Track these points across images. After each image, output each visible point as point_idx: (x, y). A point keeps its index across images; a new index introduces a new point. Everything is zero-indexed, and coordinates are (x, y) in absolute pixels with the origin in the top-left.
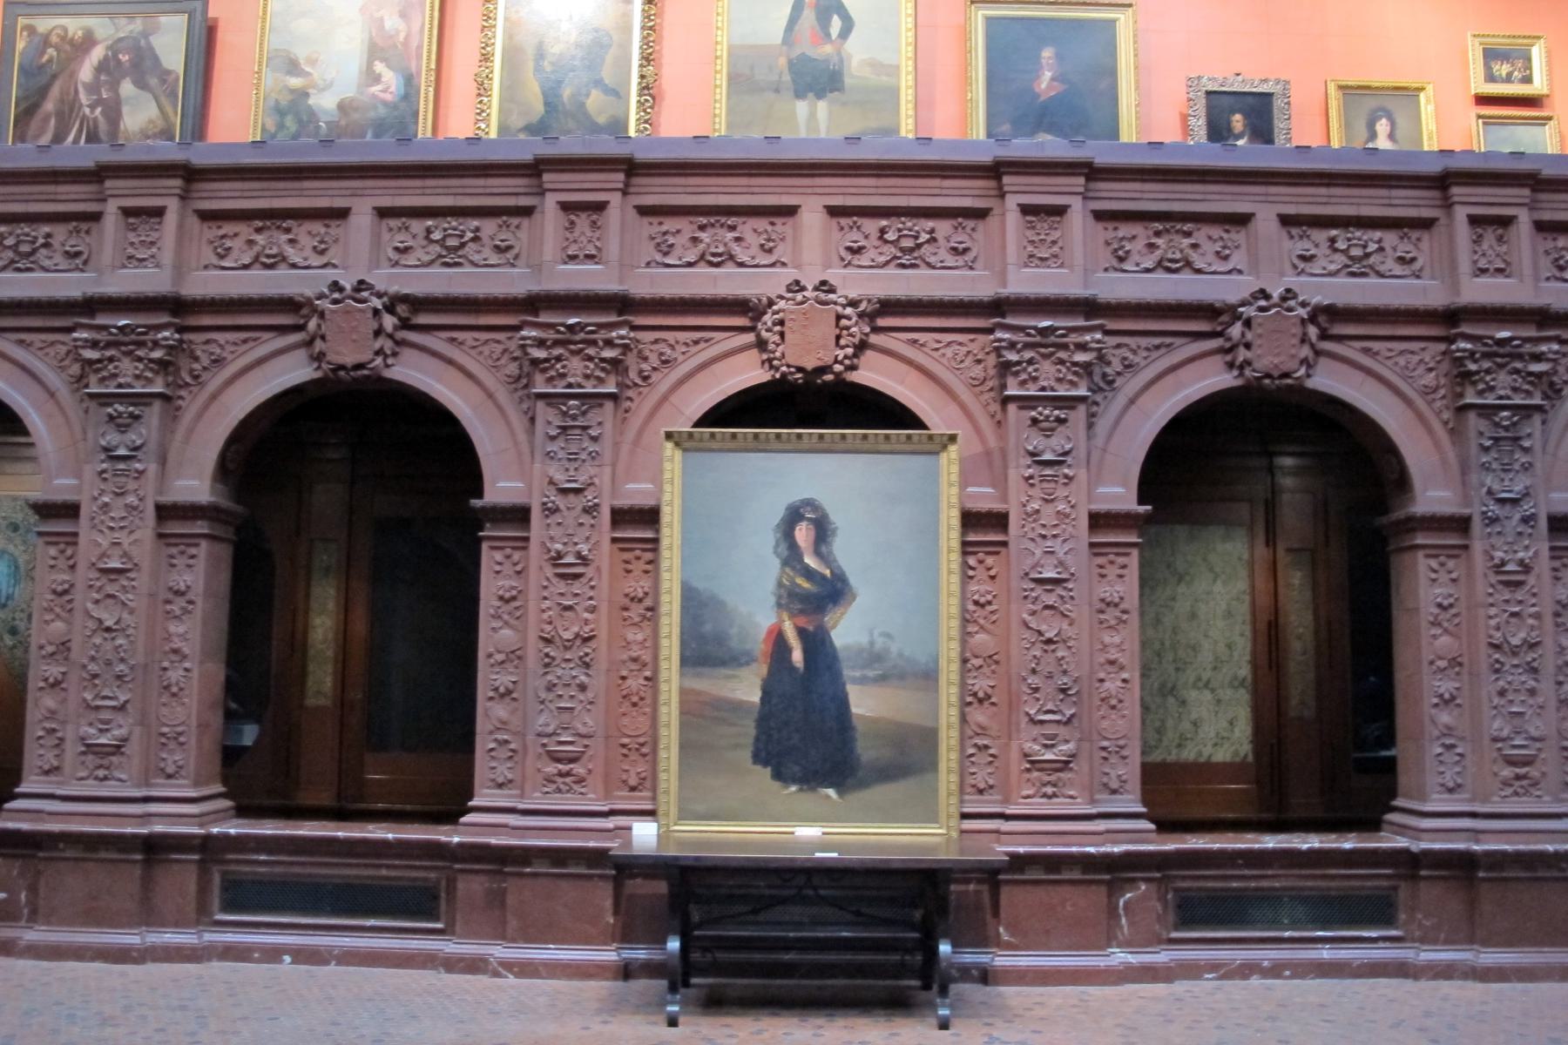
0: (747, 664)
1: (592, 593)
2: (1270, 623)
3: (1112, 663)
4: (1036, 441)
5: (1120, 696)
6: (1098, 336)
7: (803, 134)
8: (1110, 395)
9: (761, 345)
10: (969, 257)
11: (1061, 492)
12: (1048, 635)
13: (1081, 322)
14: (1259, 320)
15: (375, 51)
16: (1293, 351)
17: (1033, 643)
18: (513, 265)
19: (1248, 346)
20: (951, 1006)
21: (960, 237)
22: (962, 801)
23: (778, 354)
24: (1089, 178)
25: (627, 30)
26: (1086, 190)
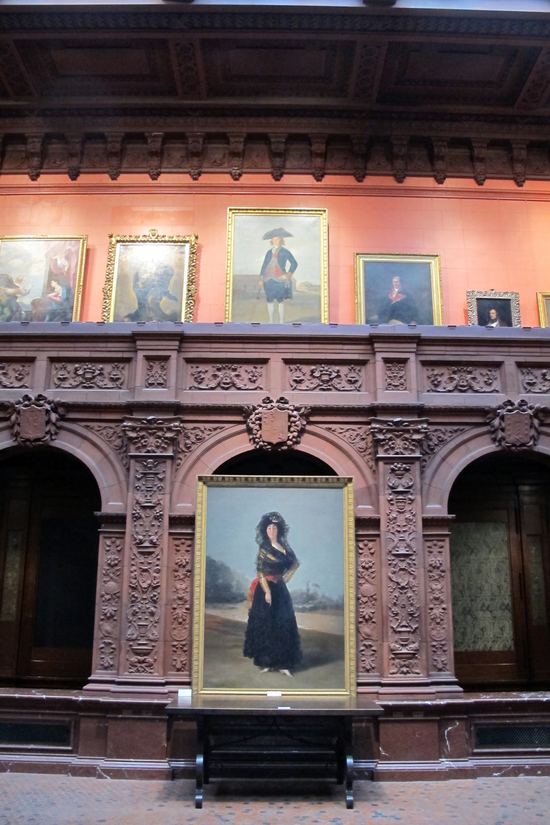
0: (241, 601)
1: (158, 563)
2: (520, 574)
3: (437, 599)
4: (394, 481)
5: (442, 617)
6: (425, 426)
7: (271, 322)
8: (432, 456)
9: (249, 431)
10: (357, 385)
11: (408, 508)
12: (402, 585)
13: (416, 419)
14: (509, 416)
15: (52, 276)
16: (526, 432)
17: (394, 589)
18: (120, 388)
19: (503, 430)
20: (354, 795)
22: (358, 676)
23: (258, 436)
24: (418, 345)
25: (182, 267)
26: (417, 350)
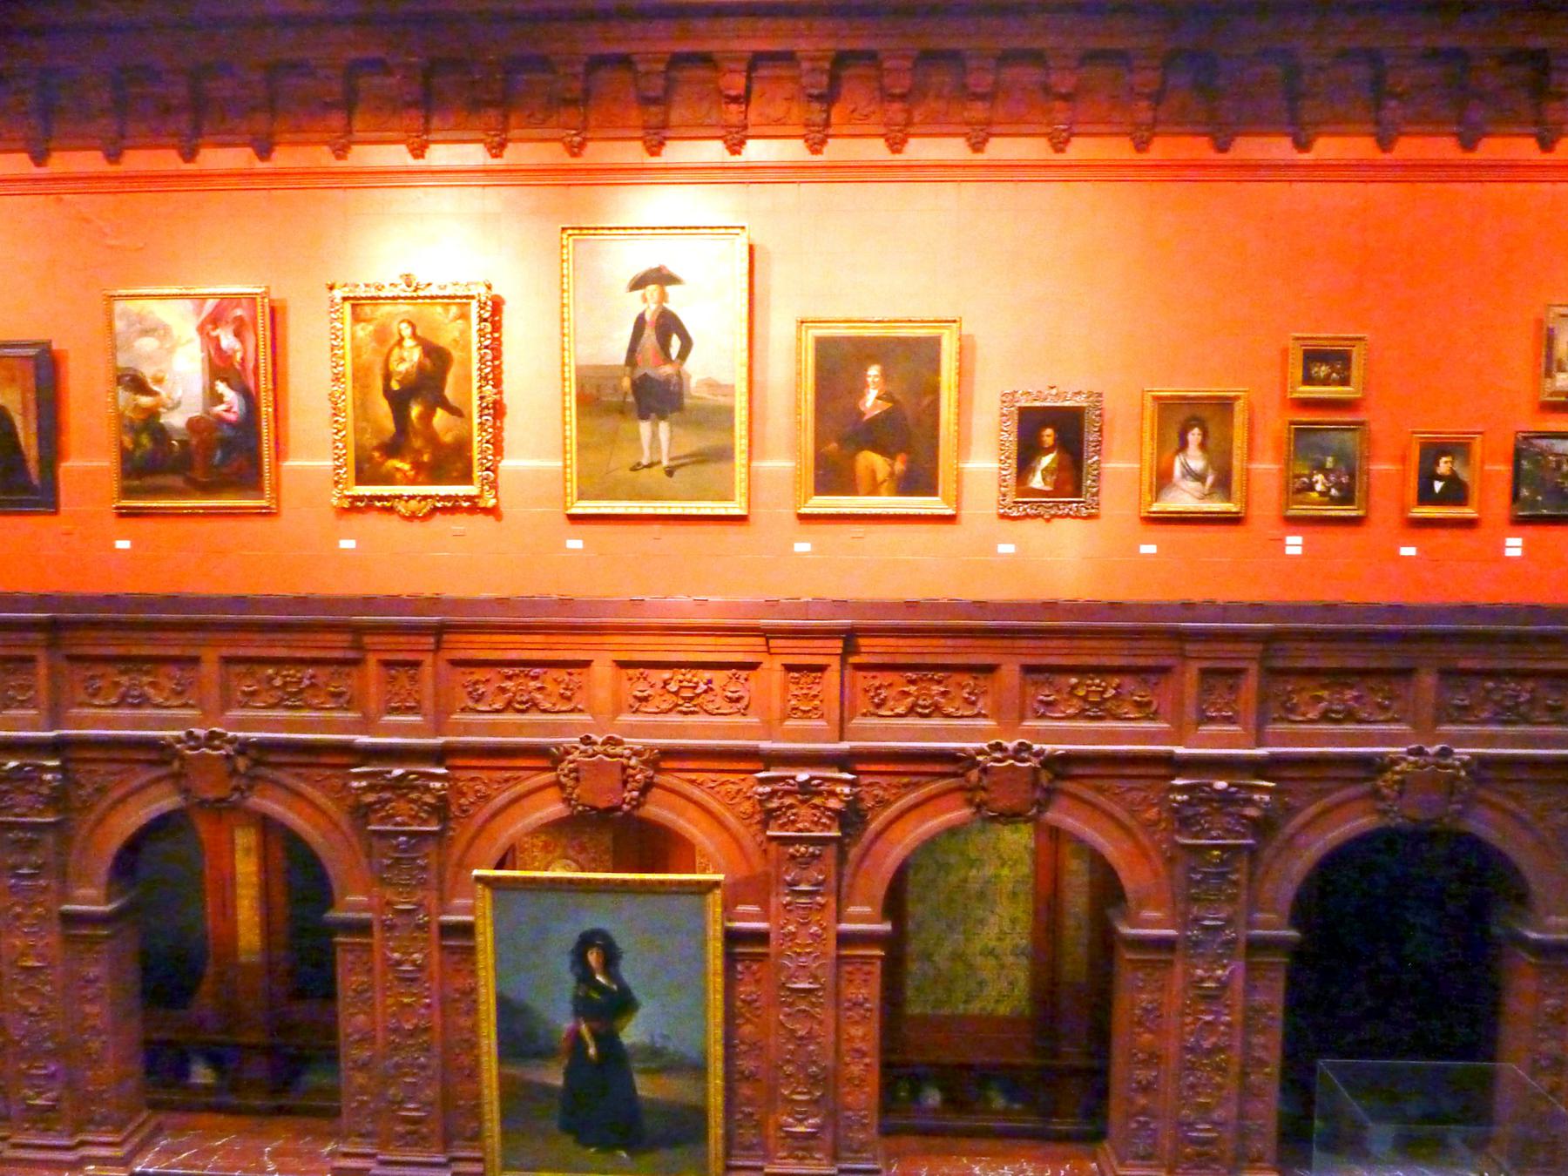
21: (734, 689)
23: (574, 796)
